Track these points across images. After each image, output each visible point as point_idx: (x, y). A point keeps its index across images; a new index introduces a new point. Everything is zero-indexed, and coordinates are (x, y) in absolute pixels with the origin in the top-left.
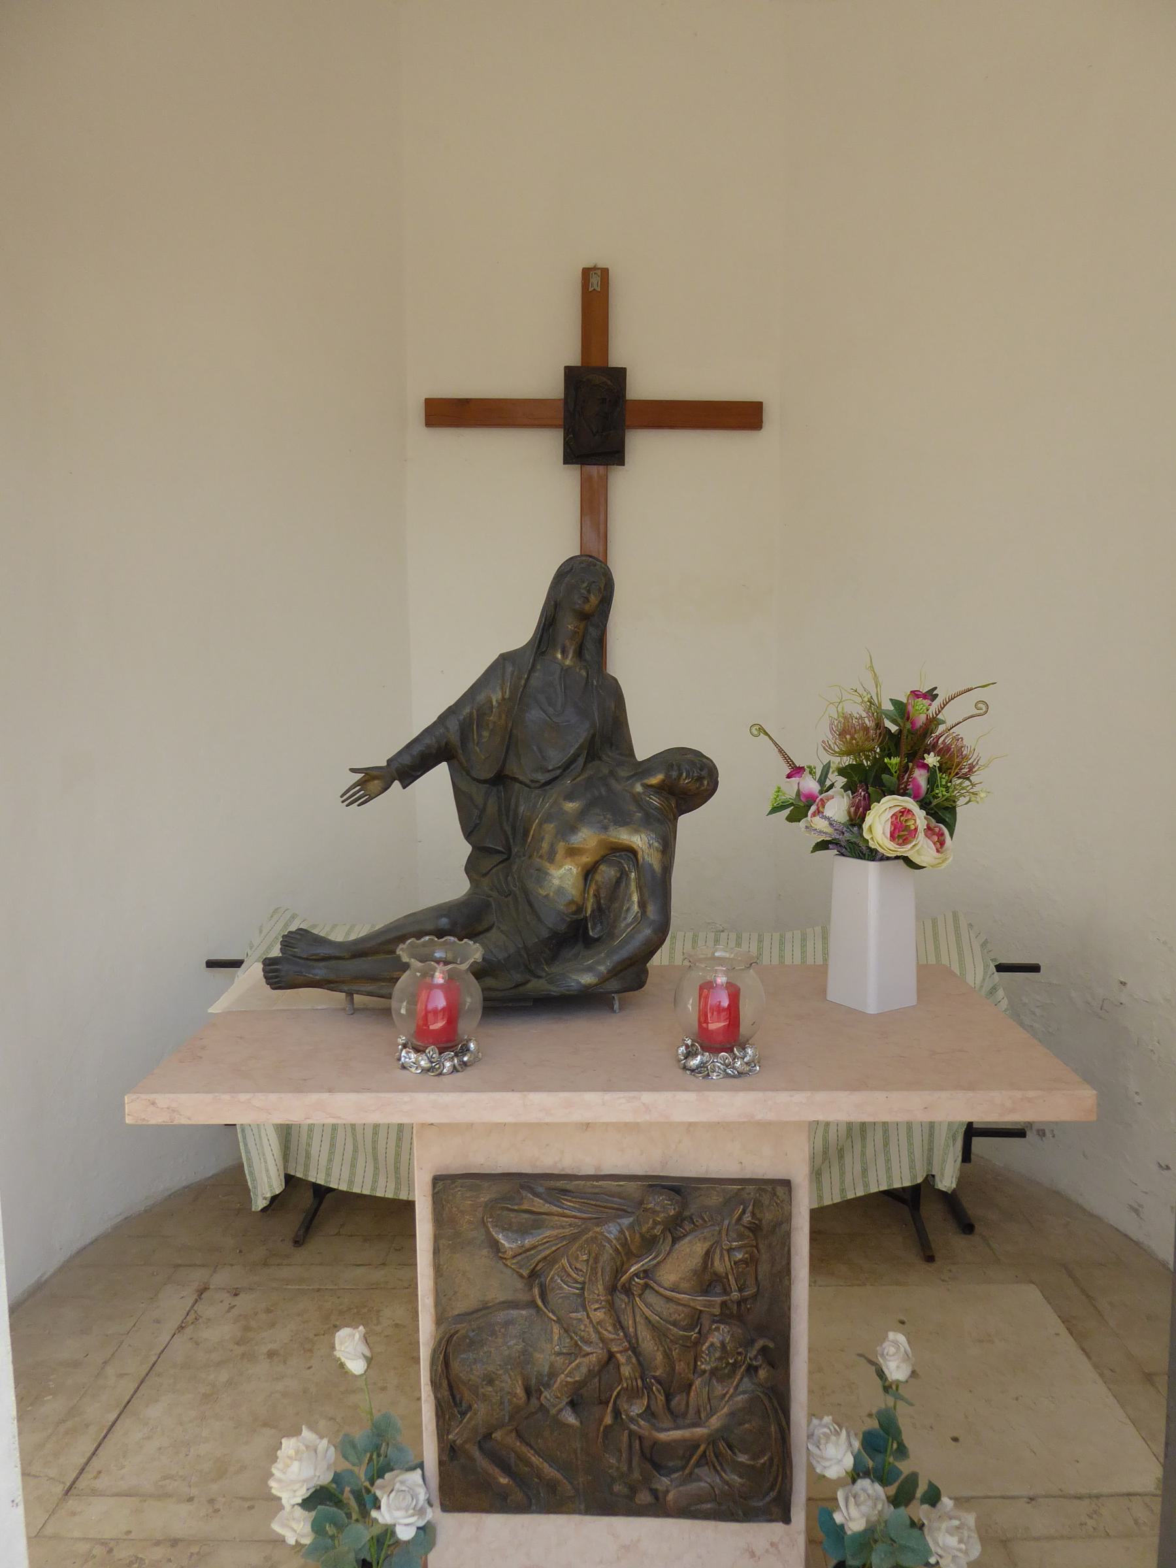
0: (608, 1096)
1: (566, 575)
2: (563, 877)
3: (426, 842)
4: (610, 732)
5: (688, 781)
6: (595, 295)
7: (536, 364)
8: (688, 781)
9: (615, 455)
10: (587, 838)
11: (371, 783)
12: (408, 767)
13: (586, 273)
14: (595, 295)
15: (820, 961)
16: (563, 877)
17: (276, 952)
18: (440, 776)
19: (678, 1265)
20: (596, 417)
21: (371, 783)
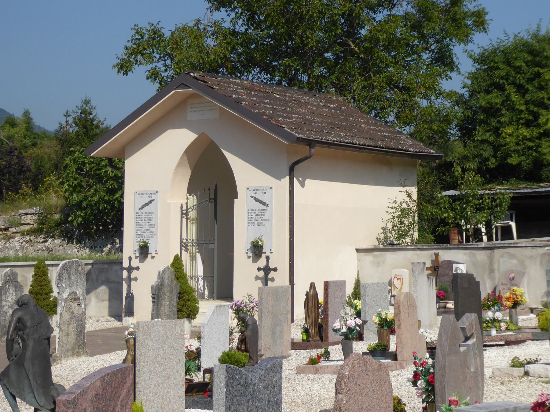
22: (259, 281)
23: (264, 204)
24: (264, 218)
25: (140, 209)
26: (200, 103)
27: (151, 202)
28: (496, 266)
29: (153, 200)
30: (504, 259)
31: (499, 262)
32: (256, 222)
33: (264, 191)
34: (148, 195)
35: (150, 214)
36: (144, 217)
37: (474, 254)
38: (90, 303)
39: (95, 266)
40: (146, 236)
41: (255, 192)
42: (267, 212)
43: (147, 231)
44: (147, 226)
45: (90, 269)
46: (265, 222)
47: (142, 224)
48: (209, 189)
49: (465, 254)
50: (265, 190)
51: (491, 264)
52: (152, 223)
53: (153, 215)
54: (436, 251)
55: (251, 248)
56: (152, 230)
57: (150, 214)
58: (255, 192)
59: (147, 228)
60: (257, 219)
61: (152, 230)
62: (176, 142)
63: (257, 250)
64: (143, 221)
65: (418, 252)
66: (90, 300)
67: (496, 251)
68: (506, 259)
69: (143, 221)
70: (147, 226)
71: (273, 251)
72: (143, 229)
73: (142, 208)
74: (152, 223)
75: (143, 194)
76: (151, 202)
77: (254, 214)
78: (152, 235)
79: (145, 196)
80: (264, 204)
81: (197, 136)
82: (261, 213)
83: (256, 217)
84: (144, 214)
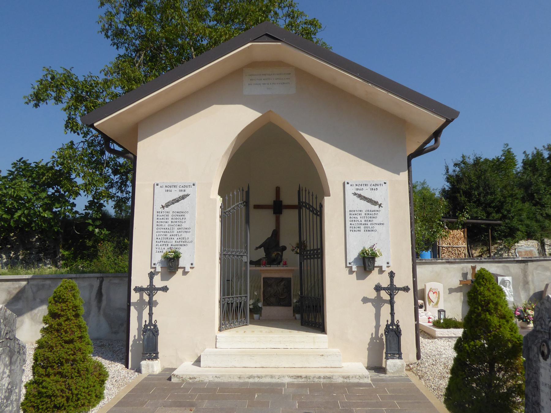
0: (449, 330)
1: (274, 231)
2: (273, 255)
3: (261, 253)
4: (278, 243)
5: (284, 248)
6: (278, 190)
7: (269, 200)
8: (284, 248)
9: (280, 213)
10: (276, 253)
11: (257, 248)
12: (260, 247)
13: (277, 188)
14: (278, 190)
15: (319, 247)
16: (273, 255)
17: (87, 204)
18: (263, 248)
19: (282, 283)
20: (278, 207)
21: (257, 248)
22: (370, 304)
23: (375, 203)
24: (375, 221)
25: (163, 207)
26: (265, 75)
27: (183, 197)
28: (530, 278)
29: (188, 195)
30: (538, 272)
31: (533, 275)
32: (362, 227)
33: (374, 187)
34: (178, 189)
35: (181, 214)
36: (170, 217)
37: (508, 267)
38: (22, 325)
39: (32, 282)
40: (174, 243)
41: (359, 187)
42: (380, 213)
43: (176, 238)
44: (176, 231)
45: (25, 287)
46: (377, 227)
47: (167, 226)
48: (243, 190)
49: (498, 267)
50: (375, 186)
51: (525, 275)
52: (184, 225)
53: (187, 216)
54: (473, 265)
55: (161, 262)
56: (184, 235)
57: (181, 214)
58: (359, 187)
59: (175, 233)
60: (363, 222)
61: (184, 235)
62: (222, 125)
63: (366, 262)
64: (170, 223)
65: (448, 266)
66: (22, 323)
67: (529, 264)
68: (540, 272)
69: (170, 223)
70: (176, 231)
71: (390, 264)
72: (169, 234)
73: (167, 205)
74: (184, 225)
75: (169, 188)
76: (183, 197)
77: (359, 217)
78: (184, 242)
79: (173, 189)
80: (375, 203)
81: (259, 115)
82: (371, 215)
83: (363, 220)
84: (170, 214)
